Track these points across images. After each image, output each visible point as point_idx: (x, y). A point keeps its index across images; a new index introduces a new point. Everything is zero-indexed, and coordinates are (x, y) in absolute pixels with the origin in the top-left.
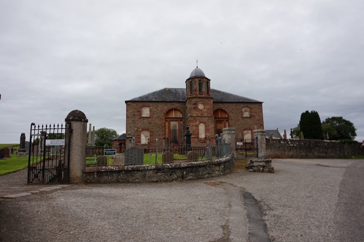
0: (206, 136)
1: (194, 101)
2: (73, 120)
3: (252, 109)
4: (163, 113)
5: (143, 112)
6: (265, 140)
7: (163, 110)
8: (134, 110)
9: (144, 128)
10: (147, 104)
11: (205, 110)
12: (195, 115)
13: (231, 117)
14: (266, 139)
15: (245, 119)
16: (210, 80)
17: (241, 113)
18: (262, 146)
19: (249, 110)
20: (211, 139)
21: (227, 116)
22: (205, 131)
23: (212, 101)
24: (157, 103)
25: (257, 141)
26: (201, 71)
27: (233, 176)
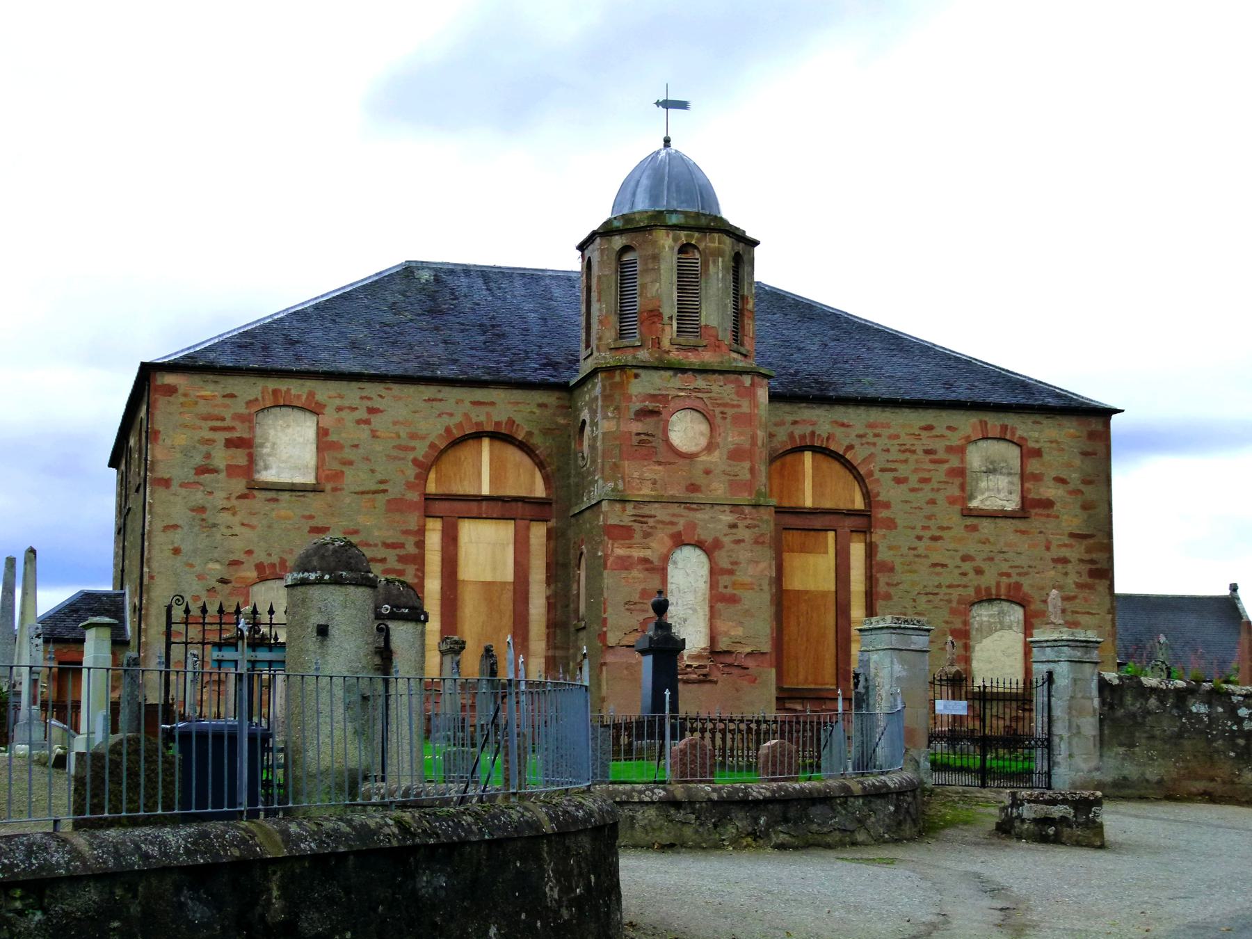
0: (713, 639)
1: (641, 387)
2: (393, 616)
3: (1038, 453)
4: (415, 461)
5: (265, 451)
6: (1095, 692)
7: (413, 436)
8: (211, 435)
9: (273, 566)
10: (297, 388)
11: (716, 457)
12: (647, 491)
13: (887, 505)
14: (1103, 685)
15: (986, 526)
16: (755, 243)
17: (958, 481)
18: (1078, 727)
19: (1016, 463)
20: (750, 663)
21: (859, 504)
22: (711, 607)
23: (763, 394)
24: (373, 389)
25: (1049, 696)
26: (691, 173)
27: (934, 846)
